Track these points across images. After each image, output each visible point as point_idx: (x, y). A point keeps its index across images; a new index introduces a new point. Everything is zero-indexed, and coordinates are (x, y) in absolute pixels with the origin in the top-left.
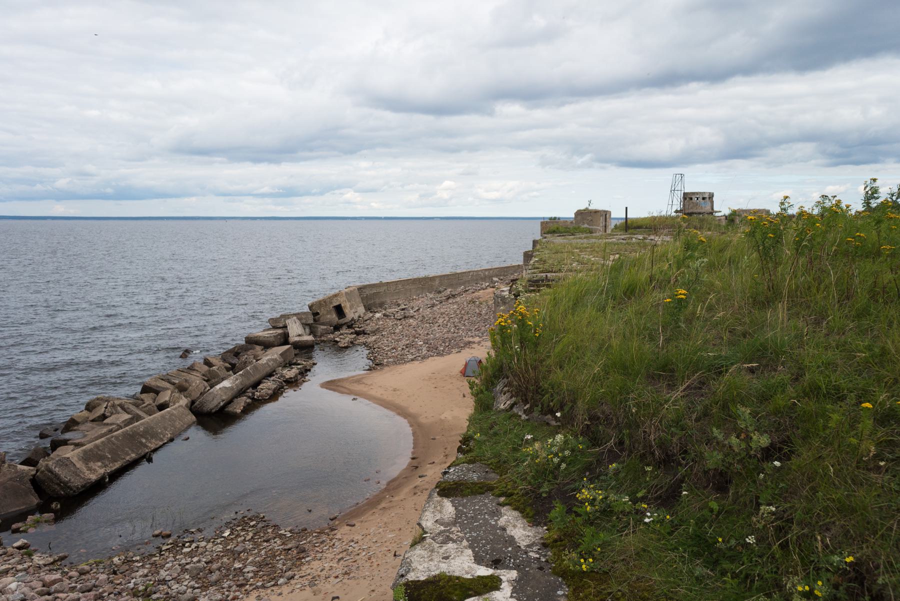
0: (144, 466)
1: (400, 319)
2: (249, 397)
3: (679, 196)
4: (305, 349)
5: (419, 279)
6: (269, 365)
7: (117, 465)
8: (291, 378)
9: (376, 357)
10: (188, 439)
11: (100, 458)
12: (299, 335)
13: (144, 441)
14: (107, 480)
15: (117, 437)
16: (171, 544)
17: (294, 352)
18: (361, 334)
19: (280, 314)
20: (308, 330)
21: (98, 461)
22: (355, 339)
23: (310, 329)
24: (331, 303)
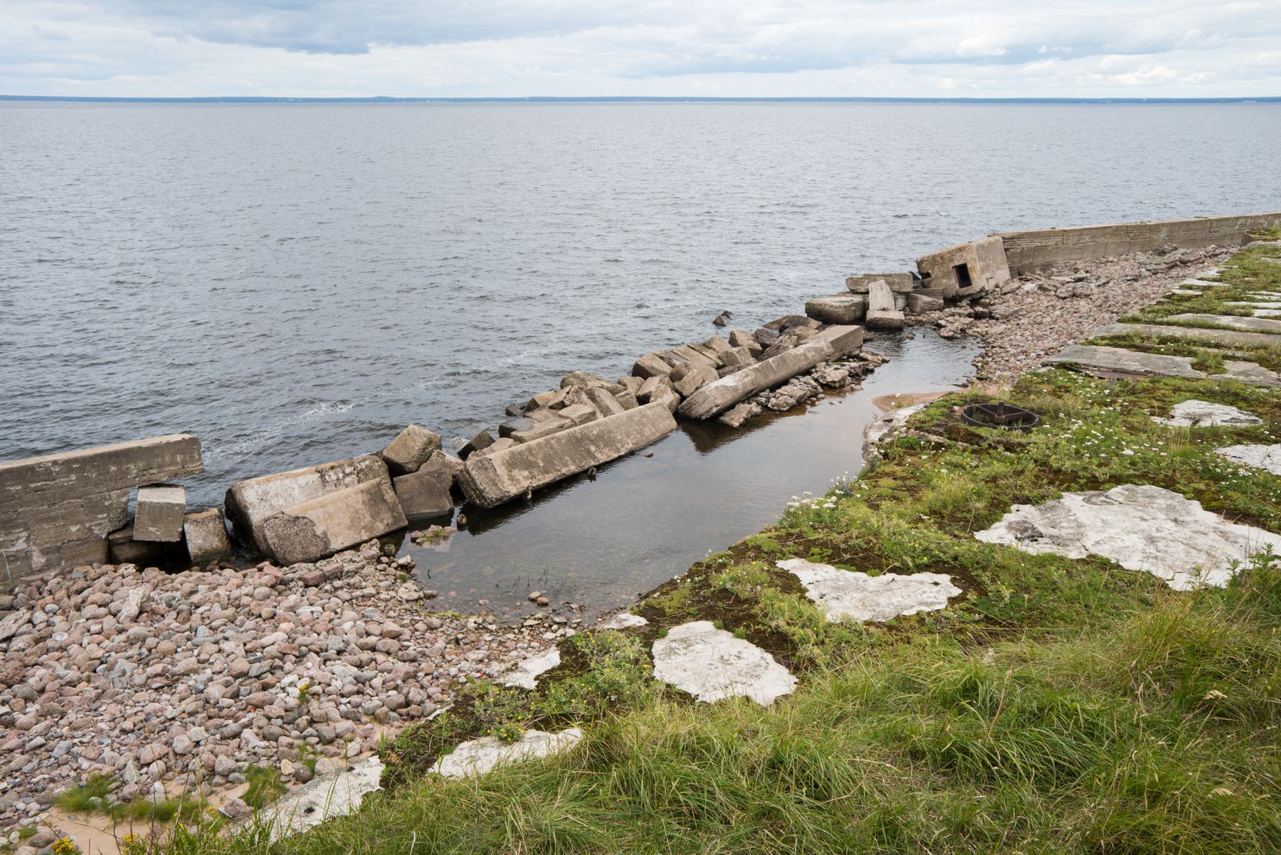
0: (585, 486)
1: (1064, 298)
2: (759, 404)
3: (720, 631)
4: (890, 331)
5: (1127, 227)
6: (806, 358)
7: (548, 478)
8: (835, 382)
9: (987, 363)
10: (650, 456)
11: (529, 465)
12: (884, 309)
13: (593, 448)
14: (530, 496)
15: (559, 440)
16: (540, 619)
17: (863, 333)
18: (984, 318)
19: (863, 272)
20: (901, 302)
21: (526, 469)
22: (971, 326)
23: (907, 299)
24: (952, 260)
